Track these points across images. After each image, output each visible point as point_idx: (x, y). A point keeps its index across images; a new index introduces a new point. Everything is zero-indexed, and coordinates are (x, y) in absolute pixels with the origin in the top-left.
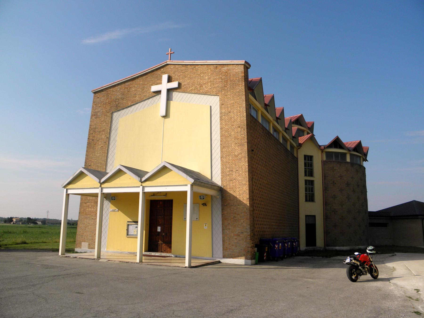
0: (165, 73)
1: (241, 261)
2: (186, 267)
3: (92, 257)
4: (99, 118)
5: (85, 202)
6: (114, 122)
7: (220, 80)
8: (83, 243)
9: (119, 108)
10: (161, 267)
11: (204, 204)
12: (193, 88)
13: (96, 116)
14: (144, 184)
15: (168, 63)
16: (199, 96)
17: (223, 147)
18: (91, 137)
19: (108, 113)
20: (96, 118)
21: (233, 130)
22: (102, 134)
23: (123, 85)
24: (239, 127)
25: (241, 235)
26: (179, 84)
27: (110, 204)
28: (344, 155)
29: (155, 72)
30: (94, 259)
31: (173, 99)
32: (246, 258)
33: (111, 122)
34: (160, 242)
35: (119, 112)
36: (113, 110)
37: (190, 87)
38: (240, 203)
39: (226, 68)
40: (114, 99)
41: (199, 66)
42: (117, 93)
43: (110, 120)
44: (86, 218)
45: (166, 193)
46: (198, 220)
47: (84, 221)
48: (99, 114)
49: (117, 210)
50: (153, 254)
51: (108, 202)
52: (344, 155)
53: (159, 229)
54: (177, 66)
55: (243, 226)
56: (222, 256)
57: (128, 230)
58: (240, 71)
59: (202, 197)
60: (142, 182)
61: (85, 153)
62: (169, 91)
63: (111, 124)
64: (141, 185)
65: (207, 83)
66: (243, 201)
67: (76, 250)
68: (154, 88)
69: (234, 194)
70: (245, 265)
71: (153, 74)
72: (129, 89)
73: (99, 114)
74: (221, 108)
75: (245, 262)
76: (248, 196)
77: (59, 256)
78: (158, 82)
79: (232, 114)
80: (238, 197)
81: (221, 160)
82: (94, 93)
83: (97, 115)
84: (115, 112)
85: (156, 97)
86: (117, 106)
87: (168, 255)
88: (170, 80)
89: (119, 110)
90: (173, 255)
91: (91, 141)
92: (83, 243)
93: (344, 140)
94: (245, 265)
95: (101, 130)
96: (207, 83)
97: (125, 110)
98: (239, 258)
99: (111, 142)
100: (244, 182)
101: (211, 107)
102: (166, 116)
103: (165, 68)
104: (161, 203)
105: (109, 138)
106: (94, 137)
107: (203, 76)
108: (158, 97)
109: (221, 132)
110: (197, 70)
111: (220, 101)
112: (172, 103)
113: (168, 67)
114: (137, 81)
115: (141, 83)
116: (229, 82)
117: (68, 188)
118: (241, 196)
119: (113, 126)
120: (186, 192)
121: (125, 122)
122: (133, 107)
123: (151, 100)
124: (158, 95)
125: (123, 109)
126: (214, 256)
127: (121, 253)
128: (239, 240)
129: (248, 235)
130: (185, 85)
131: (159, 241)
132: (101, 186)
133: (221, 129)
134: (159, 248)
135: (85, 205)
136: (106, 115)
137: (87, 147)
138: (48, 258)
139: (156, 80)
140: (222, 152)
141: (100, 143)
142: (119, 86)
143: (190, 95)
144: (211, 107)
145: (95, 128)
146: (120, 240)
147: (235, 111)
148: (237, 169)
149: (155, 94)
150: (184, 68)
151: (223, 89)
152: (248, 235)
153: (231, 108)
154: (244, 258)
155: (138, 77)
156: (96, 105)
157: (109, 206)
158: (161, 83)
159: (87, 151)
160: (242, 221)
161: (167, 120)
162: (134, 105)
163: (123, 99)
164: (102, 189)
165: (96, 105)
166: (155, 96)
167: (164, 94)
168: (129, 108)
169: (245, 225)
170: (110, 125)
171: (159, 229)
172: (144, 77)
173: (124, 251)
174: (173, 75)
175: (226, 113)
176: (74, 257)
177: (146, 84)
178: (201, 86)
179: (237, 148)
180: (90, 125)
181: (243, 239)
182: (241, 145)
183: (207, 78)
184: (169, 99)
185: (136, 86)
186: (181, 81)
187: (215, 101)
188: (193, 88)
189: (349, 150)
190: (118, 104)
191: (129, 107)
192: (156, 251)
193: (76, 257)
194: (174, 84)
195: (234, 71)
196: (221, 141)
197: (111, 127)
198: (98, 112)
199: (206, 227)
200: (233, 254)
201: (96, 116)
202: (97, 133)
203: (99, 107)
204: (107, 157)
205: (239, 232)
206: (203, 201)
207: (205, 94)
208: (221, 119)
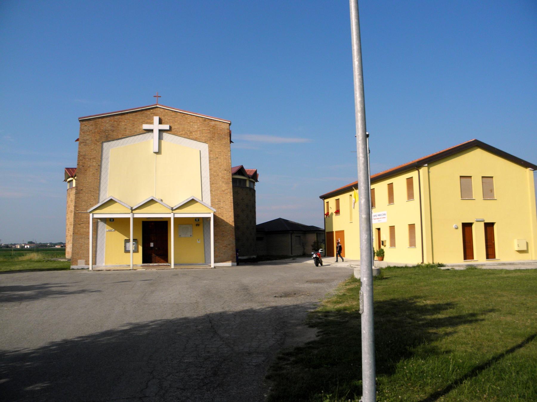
1: (229, 264)
6: (104, 151)
8: (79, 261)
15: (158, 106)
17: (212, 184)
18: (81, 164)
19: (98, 142)
20: (85, 145)
21: (220, 172)
23: (112, 118)
26: (170, 127)
28: (245, 181)
31: (164, 138)
32: (233, 262)
33: (102, 151)
34: (154, 255)
36: (103, 140)
38: (227, 224)
40: (104, 128)
42: (106, 124)
43: (100, 150)
44: (82, 238)
48: (88, 142)
52: (245, 181)
53: (152, 245)
55: (230, 240)
57: (125, 247)
62: (160, 131)
65: (196, 131)
68: (146, 126)
69: (222, 218)
71: (145, 112)
73: (88, 142)
74: (209, 153)
76: (233, 220)
78: (149, 121)
79: (219, 160)
81: (211, 193)
82: (80, 121)
88: (160, 122)
92: (79, 261)
93: (246, 168)
95: (92, 157)
96: (196, 131)
97: (115, 141)
100: (230, 210)
102: (158, 153)
103: (154, 110)
105: (100, 166)
106: (84, 163)
109: (210, 172)
112: (163, 142)
113: (157, 109)
114: (127, 116)
121: (116, 153)
123: (141, 135)
125: (113, 140)
132: (132, 212)
133: (210, 169)
134: (153, 259)
135: (79, 226)
140: (211, 187)
142: (108, 118)
145: (85, 155)
147: (222, 158)
149: (145, 132)
150: (173, 114)
151: (211, 139)
155: (127, 113)
156: (83, 132)
161: (158, 156)
162: (124, 138)
163: (113, 131)
164: (133, 214)
167: (156, 133)
168: (119, 141)
171: (152, 245)
172: (134, 114)
178: (191, 133)
179: (224, 185)
180: (79, 152)
182: (227, 183)
183: (196, 127)
184: (160, 138)
185: (126, 121)
186: (171, 125)
187: (204, 147)
188: (183, 133)
189: (249, 178)
191: (119, 139)
192: (151, 262)
194: (166, 127)
198: (87, 140)
199: (199, 242)
206: (197, 222)
207: (195, 139)
208: (210, 162)
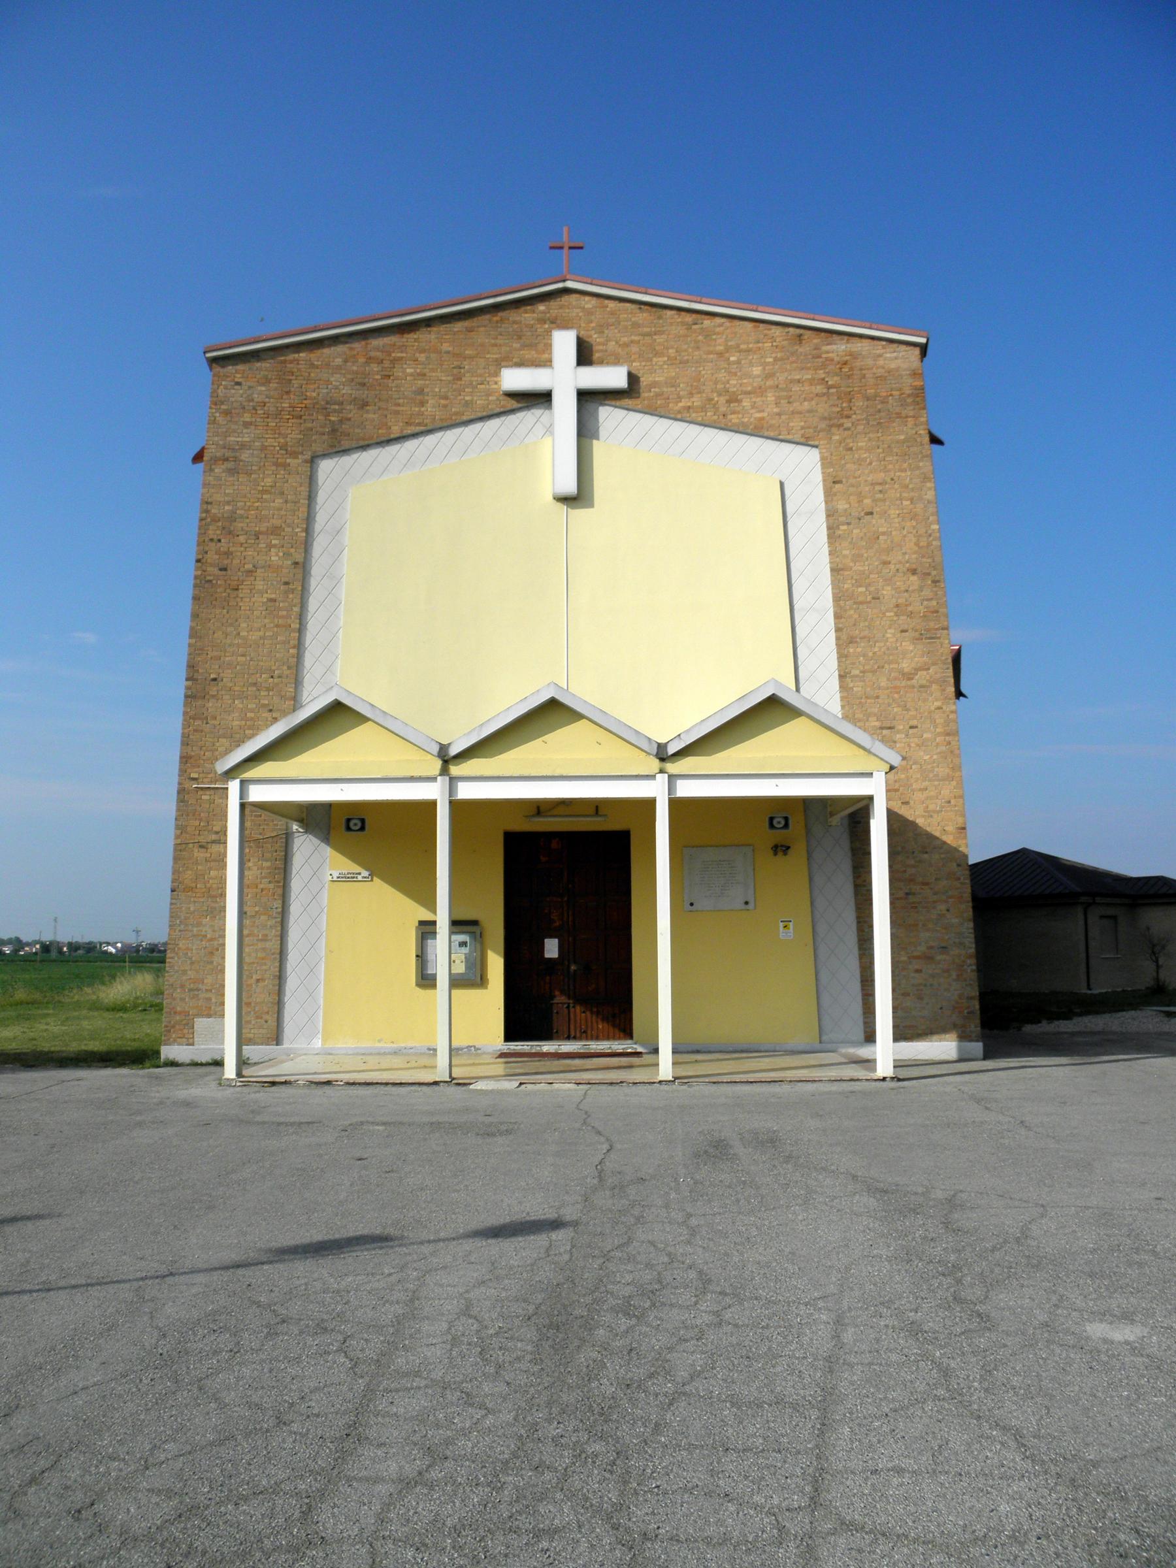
0: (565, 326)
2: (884, 1079)
3: (430, 1078)
4: (249, 474)
5: (201, 839)
6: (321, 497)
7: (820, 389)
9: (342, 442)
10: (857, 1086)
11: (780, 849)
12: (697, 401)
13: (231, 465)
14: (673, 768)
15: (570, 284)
16: (722, 437)
17: (845, 641)
18: (212, 557)
19: (294, 455)
20: (232, 472)
21: (888, 581)
22: (270, 546)
23: (358, 346)
24: (914, 572)
25: (939, 958)
26: (632, 378)
27: (328, 851)
29: (513, 315)
30: (436, 1083)
31: (603, 432)
32: (963, 1037)
33: (311, 497)
34: (560, 999)
35: (346, 460)
36: (318, 448)
37: (680, 398)
39: (840, 348)
41: (718, 320)
42: (332, 375)
45: (597, 806)
46: (751, 906)
47: (199, 924)
48: (245, 456)
49: (365, 873)
50: (547, 1047)
51: (316, 841)
53: (552, 948)
54: (612, 305)
56: (861, 1036)
58: (905, 366)
59: (779, 822)
60: (662, 760)
61: (186, 623)
62: (587, 398)
63: (309, 506)
64: (662, 771)
66: (944, 838)
67: (168, 1052)
68: (515, 379)
70: (960, 1060)
72: (387, 364)
73: (245, 456)
74: (829, 495)
75: (960, 1049)
77: (229, 1084)
78: (529, 354)
80: (920, 822)
81: (843, 687)
83: (236, 459)
84: (325, 455)
85: (520, 415)
86: (334, 431)
87: (618, 1046)
88: (584, 357)
89: (346, 452)
90: (643, 1045)
91: (216, 571)
94: (960, 1060)
95: (263, 527)
96: (760, 391)
98: (935, 1037)
99: (313, 582)
101: (782, 484)
102: (578, 498)
104: (554, 845)
105: (303, 567)
107: (738, 362)
108: (530, 417)
109: (836, 584)
110: (708, 334)
111: (823, 466)
112: (599, 449)
113: (565, 299)
115: (446, 347)
116: (859, 403)
117: (248, 775)
118: (936, 819)
119: (321, 518)
120: (432, 804)
122: (411, 444)
123: (494, 423)
124: (528, 408)
125: (364, 448)
126: (824, 1038)
127: (396, 1053)
128: (933, 976)
129: (970, 957)
130: (654, 384)
131: (552, 997)
133: (835, 570)
135: (199, 854)
136: (285, 466)
137: (195, 598)
138: (183, 1094)
139: (516, 345)
140: (842, 656)
141: (260, 585)
142: (341, 348)
143: (678, 427)
144: (782, 484)
145: (232, 518)
146: (387, 998)
147: (893, 512)
148: (914, 723)
149: (513, 404)
150: (643, 316)
151: (834, 422)
152: (970, 957)
153: (875, 501)
154: (953, 1036)
155: (428, 322)
156: (227, 413)
157: (316, 863)
158: (547, 363)
159: (195, 616)
160: (942, 907)
161: (579, 515)
162: (415, 435)
163: (364, 405)
164: (453, 781)
165: (227, 413)
166: (512, 411)
167: (565, 407)
168: (393, 449)
169: (955, 921)
170: (303, 510)
171: (552, 948)
172: (459, 326)
173: (410, 1044)
174: (595, 338)
175: (855, 513)
176: (348, 1084)
177: (471, 358)
178: (733, 399)
179: (908, 646)
181: (947, 971)
183: (757, 370)
184: (586, 431)
185: (422, 357)
187: (803, 467)
188: (697, 401)
190: (341, 421)
191: (390, 441)
192: (546, 1035)
193: (328, 1083)
194: (613, 377)
195: (881, 362)
196: (837, 616)
197: (309, 519)
198: (243, 446)
200: (910, 1027)
201: (231, 465)
202: (242, 539)
203: (247, 425)
204: (300, 646)
205: (931, 948)
206: (778, 836)
207: (756, 430)
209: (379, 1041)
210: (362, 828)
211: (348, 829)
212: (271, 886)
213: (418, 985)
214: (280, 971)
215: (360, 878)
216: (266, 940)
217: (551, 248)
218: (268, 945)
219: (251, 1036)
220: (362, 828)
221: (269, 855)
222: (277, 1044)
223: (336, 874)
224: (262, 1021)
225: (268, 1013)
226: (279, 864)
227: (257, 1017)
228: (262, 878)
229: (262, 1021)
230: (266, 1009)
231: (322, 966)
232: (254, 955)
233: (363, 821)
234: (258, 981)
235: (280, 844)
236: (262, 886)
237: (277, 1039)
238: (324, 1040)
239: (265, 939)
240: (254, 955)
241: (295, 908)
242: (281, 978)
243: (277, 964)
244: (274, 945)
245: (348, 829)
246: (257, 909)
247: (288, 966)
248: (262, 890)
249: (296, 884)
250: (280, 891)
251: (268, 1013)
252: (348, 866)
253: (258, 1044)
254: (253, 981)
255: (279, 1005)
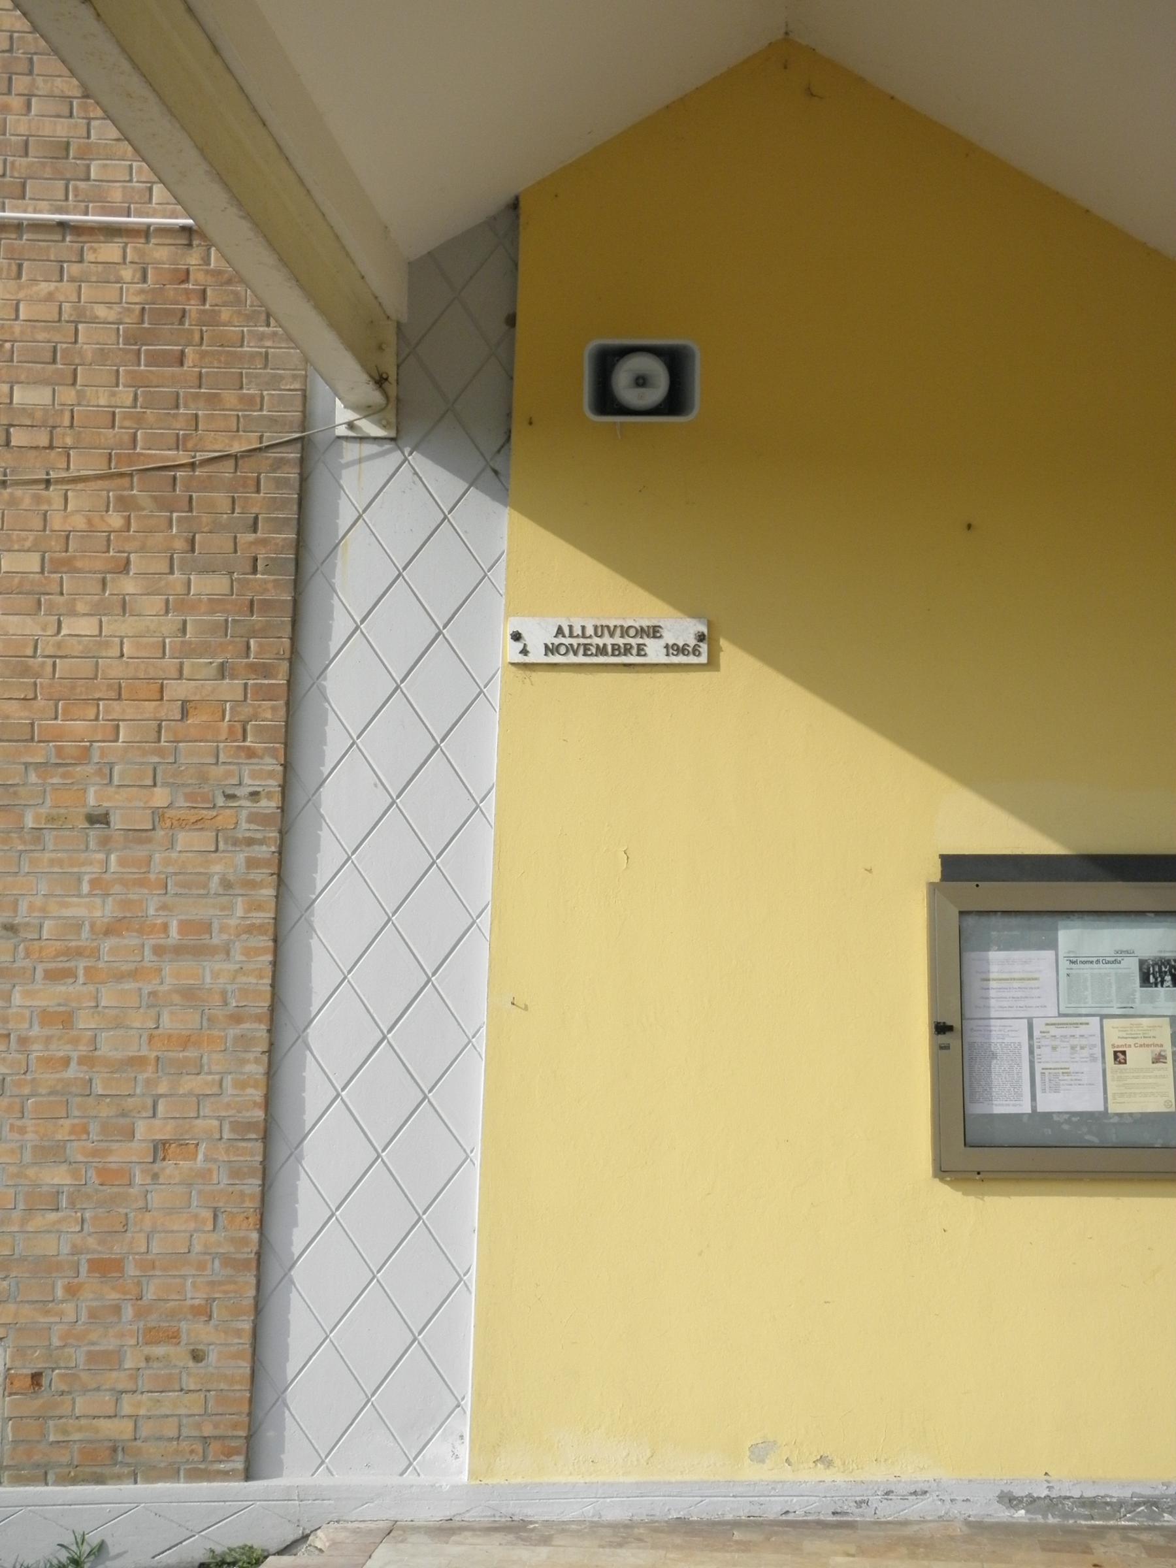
27: (501, 529)
49: (682, 629)
51: (441, 482)
209: (759, 1453)
210: (675, 402)
211: (606, 402)
212: (230, 689)
213: (944, 1170)
214: (269, 1102)
215: (655, 651)
216: (200, 952)
217: (125, 1552)
218: (213, 974)
219: (120, 1429)
220: (675, 402)
221: (222, 542)
222: (249, 1474)
223: (539, 635)
224: (178, 1354)
225: (204, 1312)
226: (271, 586)
227: (153, 1336)
228: (188, 651)
229: (178, 1354)
230: (195, 1296)
231: (477, 1072)
232: (139, 1021)
233: (676, 361)
234: (160, 1149)
235: (272, 491)
236: (177, 690)
237: (244, 1442)
238: (486, 1448)
239: (196, 944)
240: (139, 1021)
241: (342, 801)
242: (269, 1134)
243: (256, 1069)
244: (237, 973)
245: (606, 402)
246: (160, 797)
247: (311, 1073)
248: (185, 710)
249: (347, 686)
250: (271, 713)
251: (204, 1312)
252: (601, 596)
253: (154, 1473)
254: (135, 1151)
255: (261, 1266)
